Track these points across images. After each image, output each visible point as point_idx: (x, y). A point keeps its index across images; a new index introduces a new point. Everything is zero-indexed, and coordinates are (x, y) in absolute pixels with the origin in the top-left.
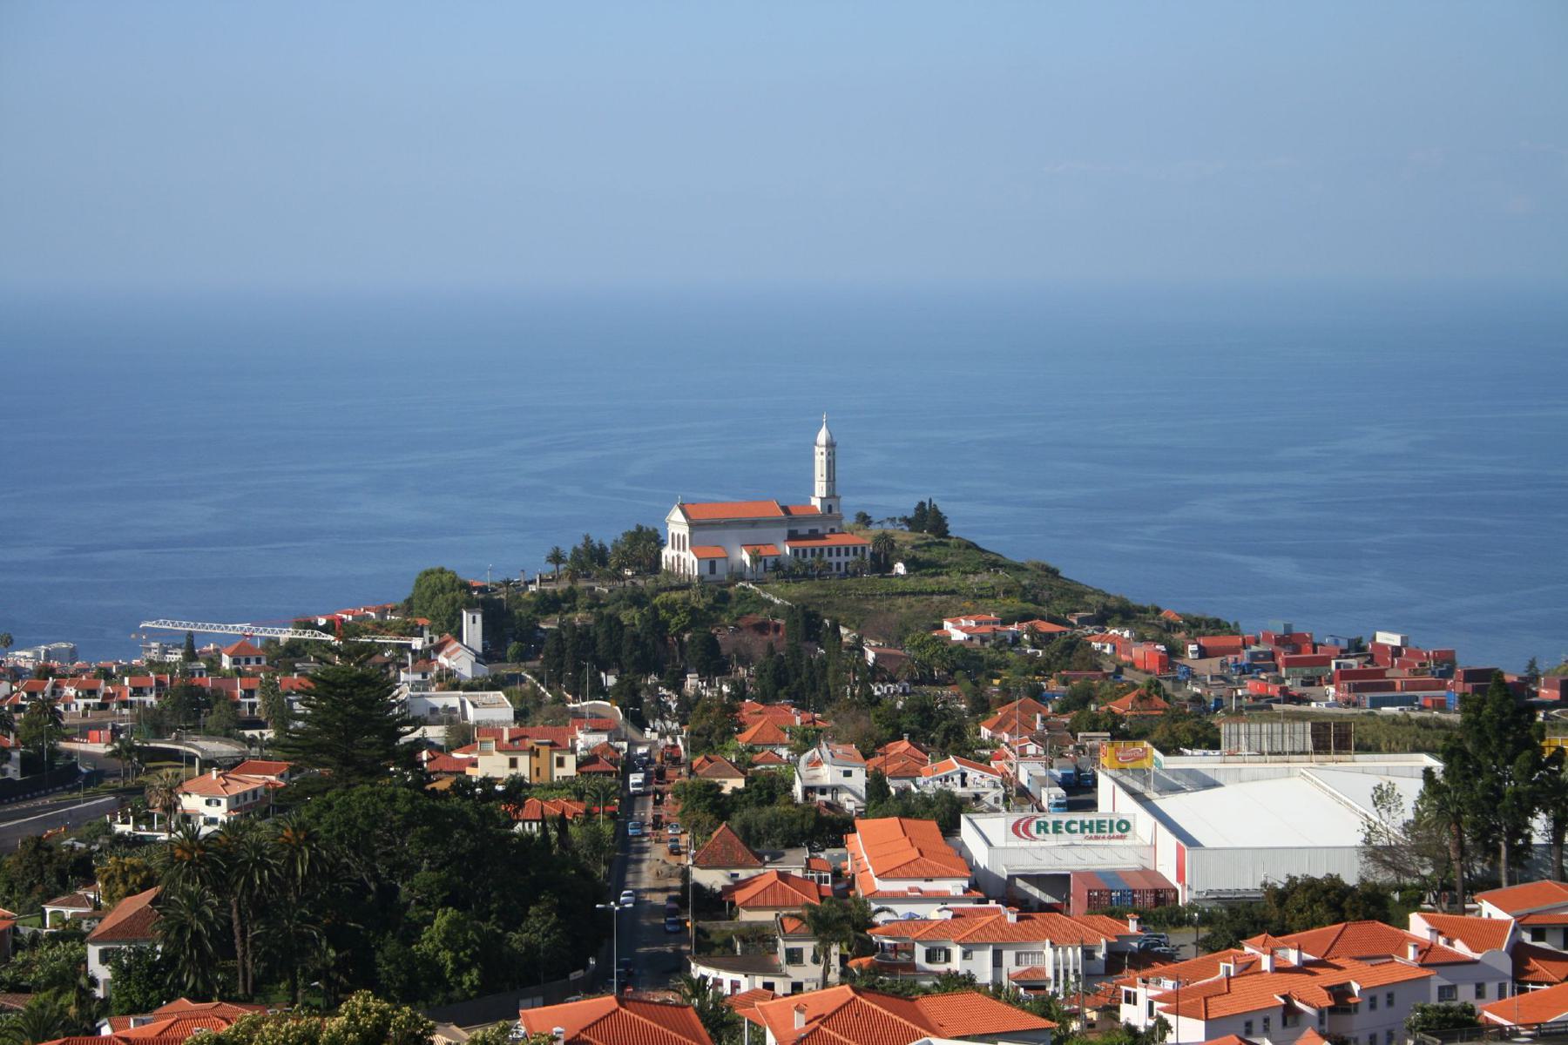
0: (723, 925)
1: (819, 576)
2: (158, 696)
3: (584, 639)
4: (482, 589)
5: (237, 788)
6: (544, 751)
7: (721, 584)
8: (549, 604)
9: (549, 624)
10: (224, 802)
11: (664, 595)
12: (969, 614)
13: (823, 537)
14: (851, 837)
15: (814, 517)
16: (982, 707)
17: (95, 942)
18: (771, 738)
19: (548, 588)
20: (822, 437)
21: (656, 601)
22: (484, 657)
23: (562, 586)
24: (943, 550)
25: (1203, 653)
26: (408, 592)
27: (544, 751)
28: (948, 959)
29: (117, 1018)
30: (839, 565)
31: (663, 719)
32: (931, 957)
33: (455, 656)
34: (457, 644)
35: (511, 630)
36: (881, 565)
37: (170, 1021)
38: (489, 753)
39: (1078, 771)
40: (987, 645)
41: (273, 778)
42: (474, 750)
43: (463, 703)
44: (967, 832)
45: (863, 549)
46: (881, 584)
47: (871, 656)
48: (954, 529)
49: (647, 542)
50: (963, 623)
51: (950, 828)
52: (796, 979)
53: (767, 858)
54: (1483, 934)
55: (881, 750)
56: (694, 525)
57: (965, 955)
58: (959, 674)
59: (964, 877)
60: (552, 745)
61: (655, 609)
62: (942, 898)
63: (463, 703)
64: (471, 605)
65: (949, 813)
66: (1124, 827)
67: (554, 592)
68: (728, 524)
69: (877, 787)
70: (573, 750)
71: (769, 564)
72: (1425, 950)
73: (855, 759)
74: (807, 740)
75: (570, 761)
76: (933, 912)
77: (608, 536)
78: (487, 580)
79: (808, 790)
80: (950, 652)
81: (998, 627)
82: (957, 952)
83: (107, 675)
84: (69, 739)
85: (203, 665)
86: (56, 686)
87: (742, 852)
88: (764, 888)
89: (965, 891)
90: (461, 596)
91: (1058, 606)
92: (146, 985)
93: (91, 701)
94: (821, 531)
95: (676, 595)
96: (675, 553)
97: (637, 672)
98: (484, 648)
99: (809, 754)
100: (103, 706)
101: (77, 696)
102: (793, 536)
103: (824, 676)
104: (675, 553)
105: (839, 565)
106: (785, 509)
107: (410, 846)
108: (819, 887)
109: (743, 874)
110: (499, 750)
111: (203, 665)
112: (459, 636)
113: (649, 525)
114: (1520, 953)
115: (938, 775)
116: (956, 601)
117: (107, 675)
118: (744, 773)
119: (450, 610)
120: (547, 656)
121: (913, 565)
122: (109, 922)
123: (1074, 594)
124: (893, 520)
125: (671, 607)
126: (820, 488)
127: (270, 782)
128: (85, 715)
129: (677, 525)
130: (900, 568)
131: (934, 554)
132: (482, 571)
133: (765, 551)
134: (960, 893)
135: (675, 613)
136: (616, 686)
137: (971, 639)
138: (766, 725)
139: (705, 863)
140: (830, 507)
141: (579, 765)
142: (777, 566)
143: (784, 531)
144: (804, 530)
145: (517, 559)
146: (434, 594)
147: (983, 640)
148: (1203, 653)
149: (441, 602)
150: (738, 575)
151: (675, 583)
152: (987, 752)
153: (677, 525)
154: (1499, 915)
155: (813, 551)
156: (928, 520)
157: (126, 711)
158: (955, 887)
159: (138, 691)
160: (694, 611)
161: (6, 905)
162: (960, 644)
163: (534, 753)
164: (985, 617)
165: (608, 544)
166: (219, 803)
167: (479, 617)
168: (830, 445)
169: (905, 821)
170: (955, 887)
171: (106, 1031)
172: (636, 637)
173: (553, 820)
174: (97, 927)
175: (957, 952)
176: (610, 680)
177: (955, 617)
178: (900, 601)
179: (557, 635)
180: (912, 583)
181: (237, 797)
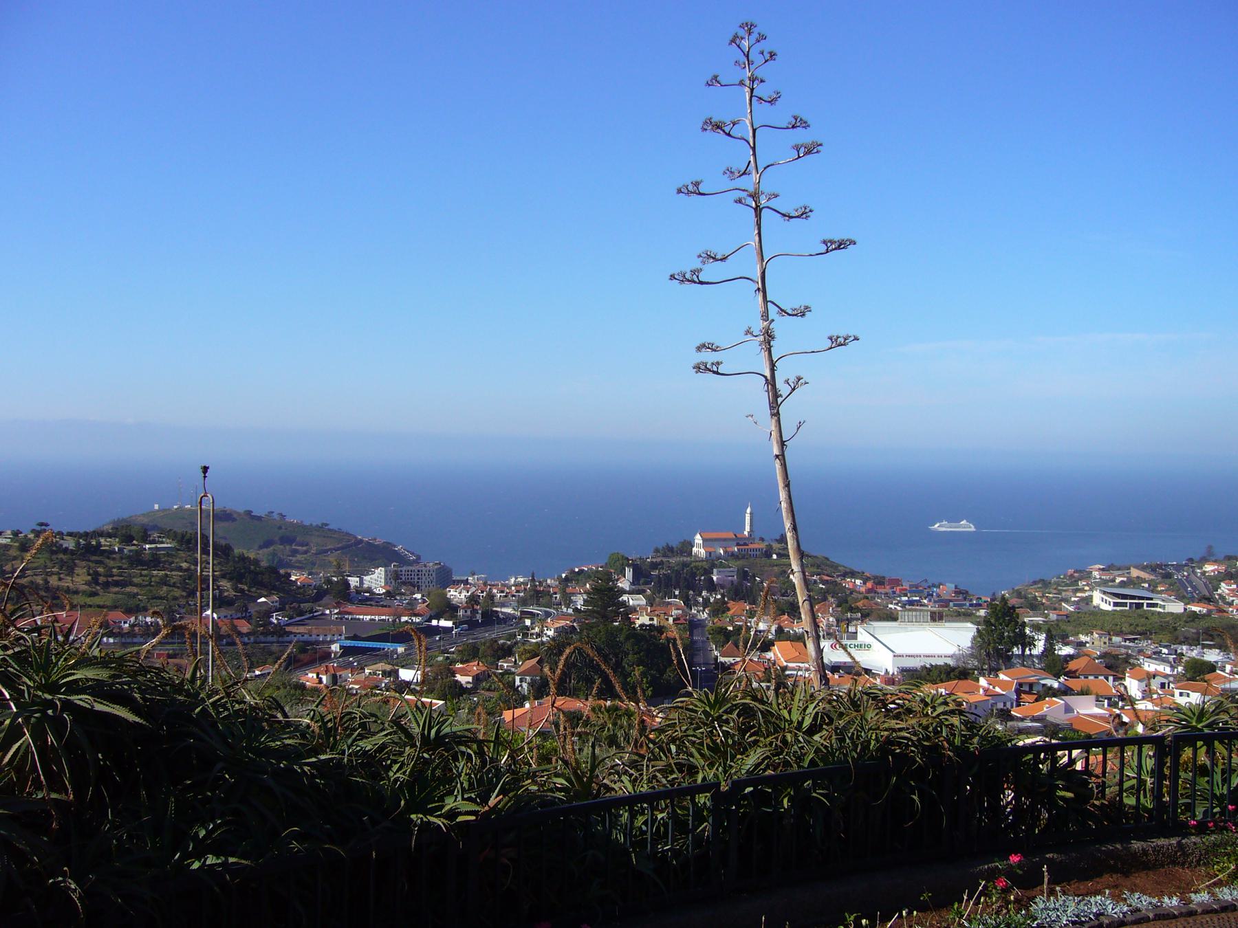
8: (654, 566)
20: (749, 510)
22: (633, 584)
23: (659, 560)
25: (1181, 694)
35: (641, 575)
54: (1003, 685)
64: (629, 566)
66: (869, 646)
69: (780, 630)
72: (986, 690)
74: (752, 614)
75: (671, 619)
77: (675, 544)
91: (829, 571)
102: (738, 544)
107: (628, 646)
113: (688, 539)
114: (1018, 692)
123: (835, 567)
126: (747, 528)
129: (698, 539)
130: (775, 557)
132: (633, 556)
138: (735, 607)
142: (733, 554)
148: (1181, 694)
149: (620, 562)
150: (719, 557)
153: (698, 539)
154: (1006, 678)
161: (1235, 690)
176: (677, 593)
179: (658, 576)
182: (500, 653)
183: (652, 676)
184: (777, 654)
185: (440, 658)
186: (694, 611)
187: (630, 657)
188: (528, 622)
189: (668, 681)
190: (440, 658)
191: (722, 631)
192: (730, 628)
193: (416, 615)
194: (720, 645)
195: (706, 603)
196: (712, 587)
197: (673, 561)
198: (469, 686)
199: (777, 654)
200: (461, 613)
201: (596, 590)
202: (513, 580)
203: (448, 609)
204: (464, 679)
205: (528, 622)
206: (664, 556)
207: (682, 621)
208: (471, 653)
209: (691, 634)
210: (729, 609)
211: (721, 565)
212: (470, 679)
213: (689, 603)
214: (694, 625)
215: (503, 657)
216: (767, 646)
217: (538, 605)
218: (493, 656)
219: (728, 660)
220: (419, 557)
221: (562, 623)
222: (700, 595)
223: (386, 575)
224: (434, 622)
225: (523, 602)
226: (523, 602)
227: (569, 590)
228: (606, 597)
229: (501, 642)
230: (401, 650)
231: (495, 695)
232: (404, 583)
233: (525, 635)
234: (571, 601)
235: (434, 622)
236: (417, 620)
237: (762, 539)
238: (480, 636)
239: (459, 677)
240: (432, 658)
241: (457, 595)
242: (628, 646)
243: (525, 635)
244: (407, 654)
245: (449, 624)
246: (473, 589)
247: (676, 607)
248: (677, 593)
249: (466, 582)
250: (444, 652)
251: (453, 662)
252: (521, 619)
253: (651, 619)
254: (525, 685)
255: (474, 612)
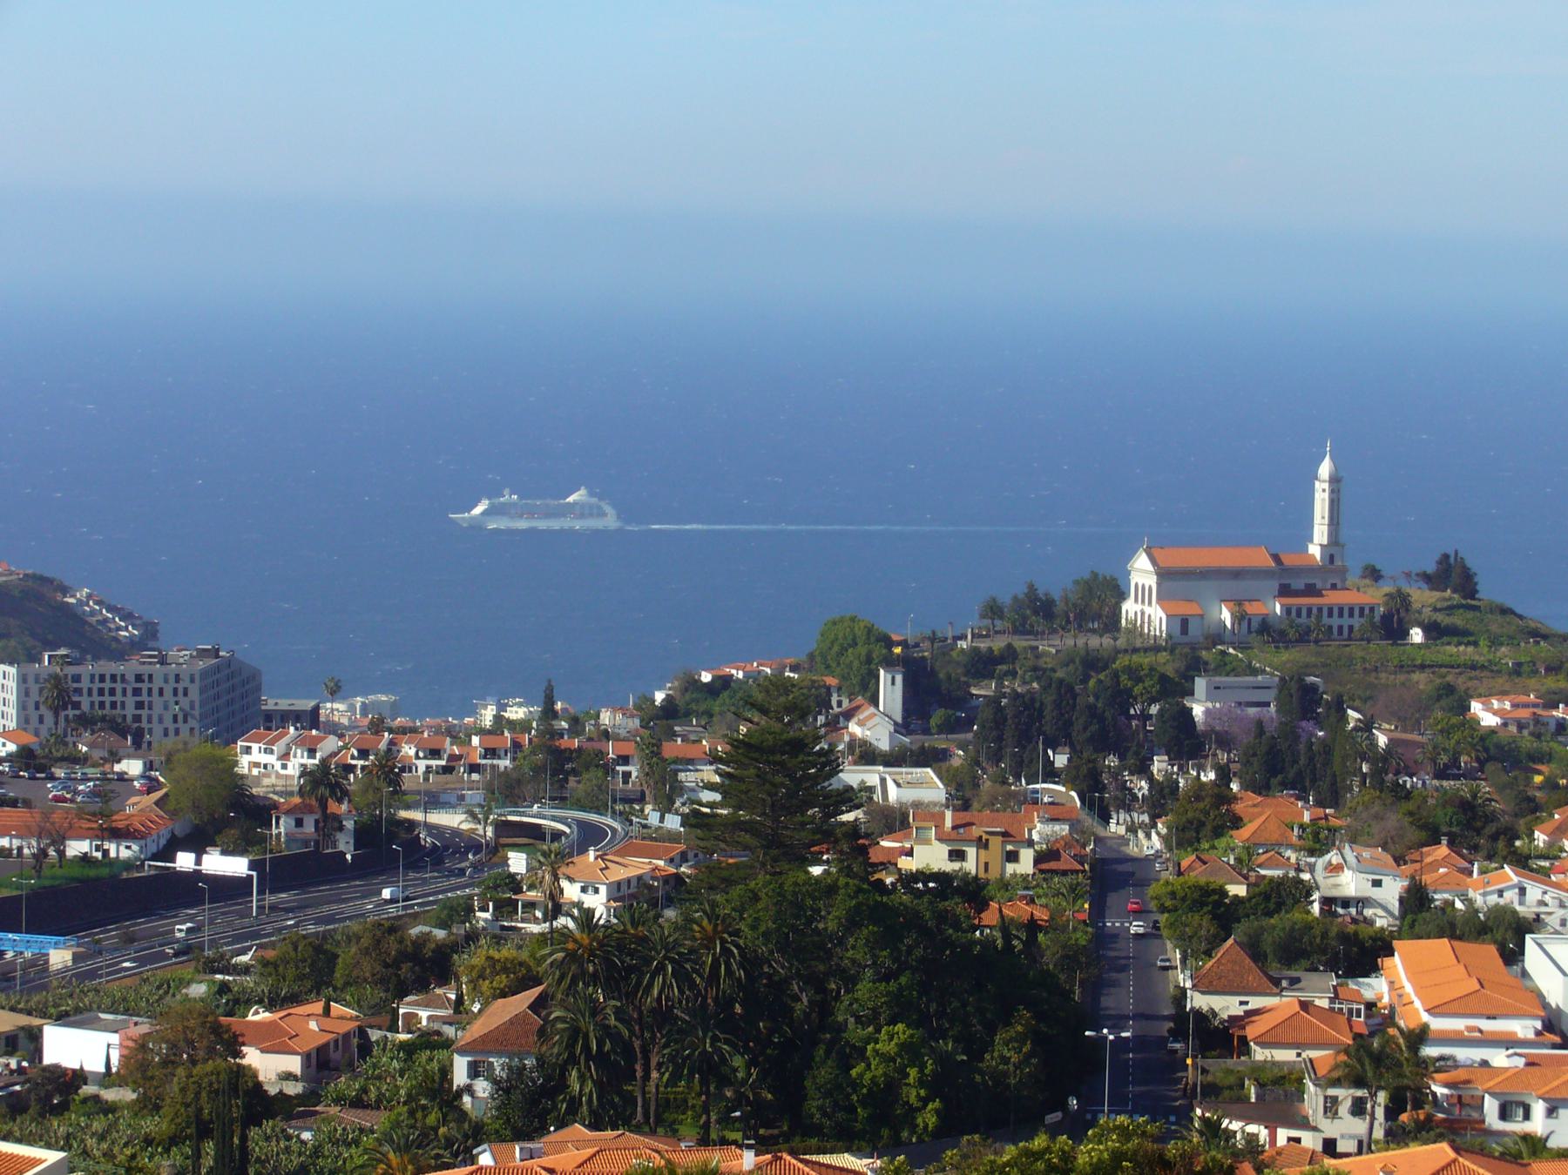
0: (1231, 1062)
1: (1316, 642)
2: (514, 759)
3: (1028, 707)
4: (904, 644)
5: (619, 874)
6: (995, 842)
7: (1194, 648)
8: (983, 665)
9: (982, 690)
10: (603, 889)
11: (1127, 658)
12: (1502, 694)
13: (1319, 594)
14: (1387, 962)
15: (1312, 569)
16: (1532, 809)
17: (463, 1052)
18: (1275, 837)
19: (983, 645)
20: (1325, 469)
21: (1116, 665)
22: (903, 728)
23: (998, 644)
24: (1470, 614)
26: (813, 646)
27: (995, 842)
28: (1527, 1117)
29: (497, 1146)
30: (1340, 628)
31: (1129, 810)
32: (1504, 1114)
33: (870, 724)
34: (872, 709)
35: (931, 696)
36: (1393, 629)
37: (591, 1151)
38: (927, 842)
39: (1064, 947)
40: (1525, 732)
41: (661, 863)
42: (908, 837)
43: (883, 781)
44: (1533, 957)
45: (1372, 609)
46: (1394, 653)
47: (1382, 740)
48: (1488, 591)
49: (1107, 592)
50: (1496, 704)
51: (1513, 956)
52: (1329, 1134)
53: (1284, 983)
55: (1416, 856)
56: (1164, 574)
57: (1551, 1112)
58: (1489, 767)
59: (1535, 1017)
60: (1005, 834)
61: (1116, 675)
62: (1508, 1042)
63: (883, 781)
64: (889, 663)
65: (1509, 935)
67: (990, 649)
68: (1205, 574)
69: (1416, 899)
70: (1030, 843)
71: (1255, 625)
73: (1386, 865)
74: (1318, 840)
76: (1500, 1058)
77: (1058, 583)
78: (908, 633)
79: (1327, 902)
80: (1482, 739)
81: (1539, 711)
82: (1539, 1108)
83: (452, 733)
84: (408, 807)
85: (564, 725)
86: (392, 743)
87: (1254, 975)
88: (1278, 1018)
89: (1538, 1033)
90: (879, 651)
92: (530, 1111)
93: (434, 763)
94: (1319, 586)
95: (1146, 660)
96: (1138, 607)
97: (1096, 750)
98: (904, 718)
99: (1327, 857)
100: (448, 770)
101: (417, 757)
102: (1285, 591)
103: (1327, 763)
104: (1138, 607)
105: (1340, 628)
106: (1276, 558)
107: (856, 951)
108: (1349, 1020)
109: (1255, 1002)
110: (940, 839)
111: (564, 725)
112: (874, 701)
113: (1105, 571)
115: (1493, 889)
116: (1490, 678)
117: (452, 733)
118: (1246, 877)
119: (864, 671)
120: (982, 727)
121: (1434, 631)
122: (477, 1029)
124: (1408, 575)
125: (1134, 674)
126: (1320, 533)
127: (657, 868)
128: (426, 779)
129: (1142, 571)
130: (1417, 635)
131: (1457, 620)
132: (903, 631)
133: (1252, 609)
134: (1531, 1035)
135: (1140, 680)
136: (1067, 767)
137: (1505, 725)
138: (1264, 816)
139: (1206, 985)
140: (1332, 558)
141: (1037, 862)
142: (1265, 628)
143: (1274, 585)
144: (1298, 584)
145: (947, 611)
146: (843, 650)
147: (1521, 727)
149: (858, 655)
150: (1217, 636)
151: (1138, 644)
152: (1546, 864)
153: (1142, 571)
155: (1309, 611)
156: (1453, 575)
157: (475, 776)
158: (1524, 1028)
159: (490, 752)
160: (1163, 678)
162: (1492, 731)
163: (982, 844)
164: (1523, 699)
165: (1056, 595)
166: (596, 891)
167: (899, 678)
168: (1335, 480)
169: (1456, 944)
170: (1524, 1028)
171: (486, 1159)
172: (1091, 709)
173: (1020, 926)
174: (471, 1035)
175: (1539, 1108)
176: (1061, 760)
177: (1485, 696)
178: (1416, 676)
179: (994, 701)
180: (1430, 656)
181: (619, 884)
182: (405, 970)
183: (943, 1060)
184: (1401, 985)
185: (198, 990)
186: (1116, 828)
187: (863, 989)
188: (517, 862)
189: (999, 1078)
190: (198, 990)
191: (1209, 900)
192: (1238, 890)
193: (118, 834)
194: (1198, 949)
195: (1162, 799)
196: (1187, 741)
197: (1048, 647)
198: (293, 1089)
199: (1401, 985)
200: (282, 827)
201: (744, 751)
202: (488, 715)
203: (236, 814)
204: (270, 1067)
205: (517, 862)
206: (1021, 629)
207: (1066, 862)
208: (310, 972)
209: (1098, 911)
210: (1237, 822)
211: (1224, 666)
212: (294, 1064)
213: (1100, 800)
214: (1110, 876)
215: (421, 986)
216: (1361, 953)
217: (561, 800)
218: (382, 981)
219: (1227, 1006)
220: (150, 632)
221: (637, 866)
222: (1143, 770)
223: (24, 693)
224: (185, 861)
225: (509, 790)
226: (509, 790)
227: (674, 748)
228: (784, 769)
229: (415, 931)
230: (60, 956)
231: (378, 1121)
232: (85, 722)
233: (506, 908)
234: (678, 788)
235: (185, 861)
236: (121, 851)
237: (1374, 574)
238: (347, 908)
239: (252, 1057)
240: (167, 987)
241: (269, 764)
242: (856, 951)
243: (506, 908)
244: (80, 975)
245: (237, 866)
246: (331, 744)
247: (1048, 817)
248: (1061, 760)
249: (311, 719)
250: (211, 967)
251: (240, 1003)
252: (495, 851)
253: (957, 855)
254: (482, 1087)
255: (329, 824)
